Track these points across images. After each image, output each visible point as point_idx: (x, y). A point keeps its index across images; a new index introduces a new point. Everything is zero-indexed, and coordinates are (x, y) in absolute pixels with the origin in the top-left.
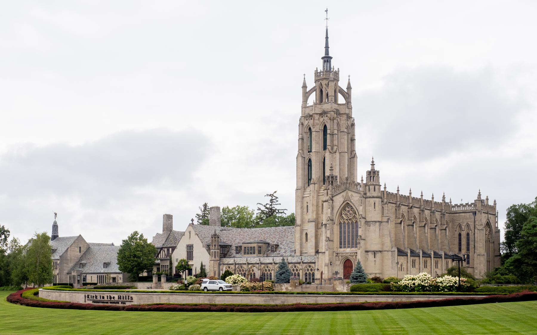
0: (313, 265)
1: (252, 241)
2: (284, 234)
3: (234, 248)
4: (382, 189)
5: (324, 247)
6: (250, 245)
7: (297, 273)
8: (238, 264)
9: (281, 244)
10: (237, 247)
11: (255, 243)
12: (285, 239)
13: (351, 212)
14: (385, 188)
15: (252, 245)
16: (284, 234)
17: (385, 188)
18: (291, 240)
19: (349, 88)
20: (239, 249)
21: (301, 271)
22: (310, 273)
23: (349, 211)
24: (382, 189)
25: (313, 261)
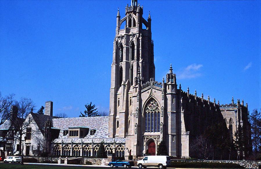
0: (124, 145)
1: (76, 127)
2: (100, 122)
3: (63, 132)
4: (178, 88)
5: (133, 131)
6: (74, 130)
7: (78, 150)
8: (85, 144)
9: (98, 129)
10: (64, 131)
11: (173, 99)
12: (101, 125)
13: (154, 104)
14: (180, 87)
15: (76, 130)
16: (100, 122)
17: (180, 87)
18: (106, 127)
19: (150, 20)
20: (65, 133)
21: (81, 149)
22: (120, 151)
23: (152, 104)
24: (178, 88)
25: (124, 142)
